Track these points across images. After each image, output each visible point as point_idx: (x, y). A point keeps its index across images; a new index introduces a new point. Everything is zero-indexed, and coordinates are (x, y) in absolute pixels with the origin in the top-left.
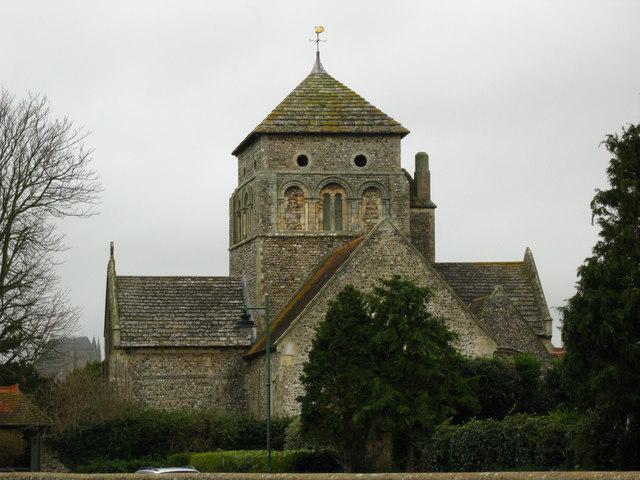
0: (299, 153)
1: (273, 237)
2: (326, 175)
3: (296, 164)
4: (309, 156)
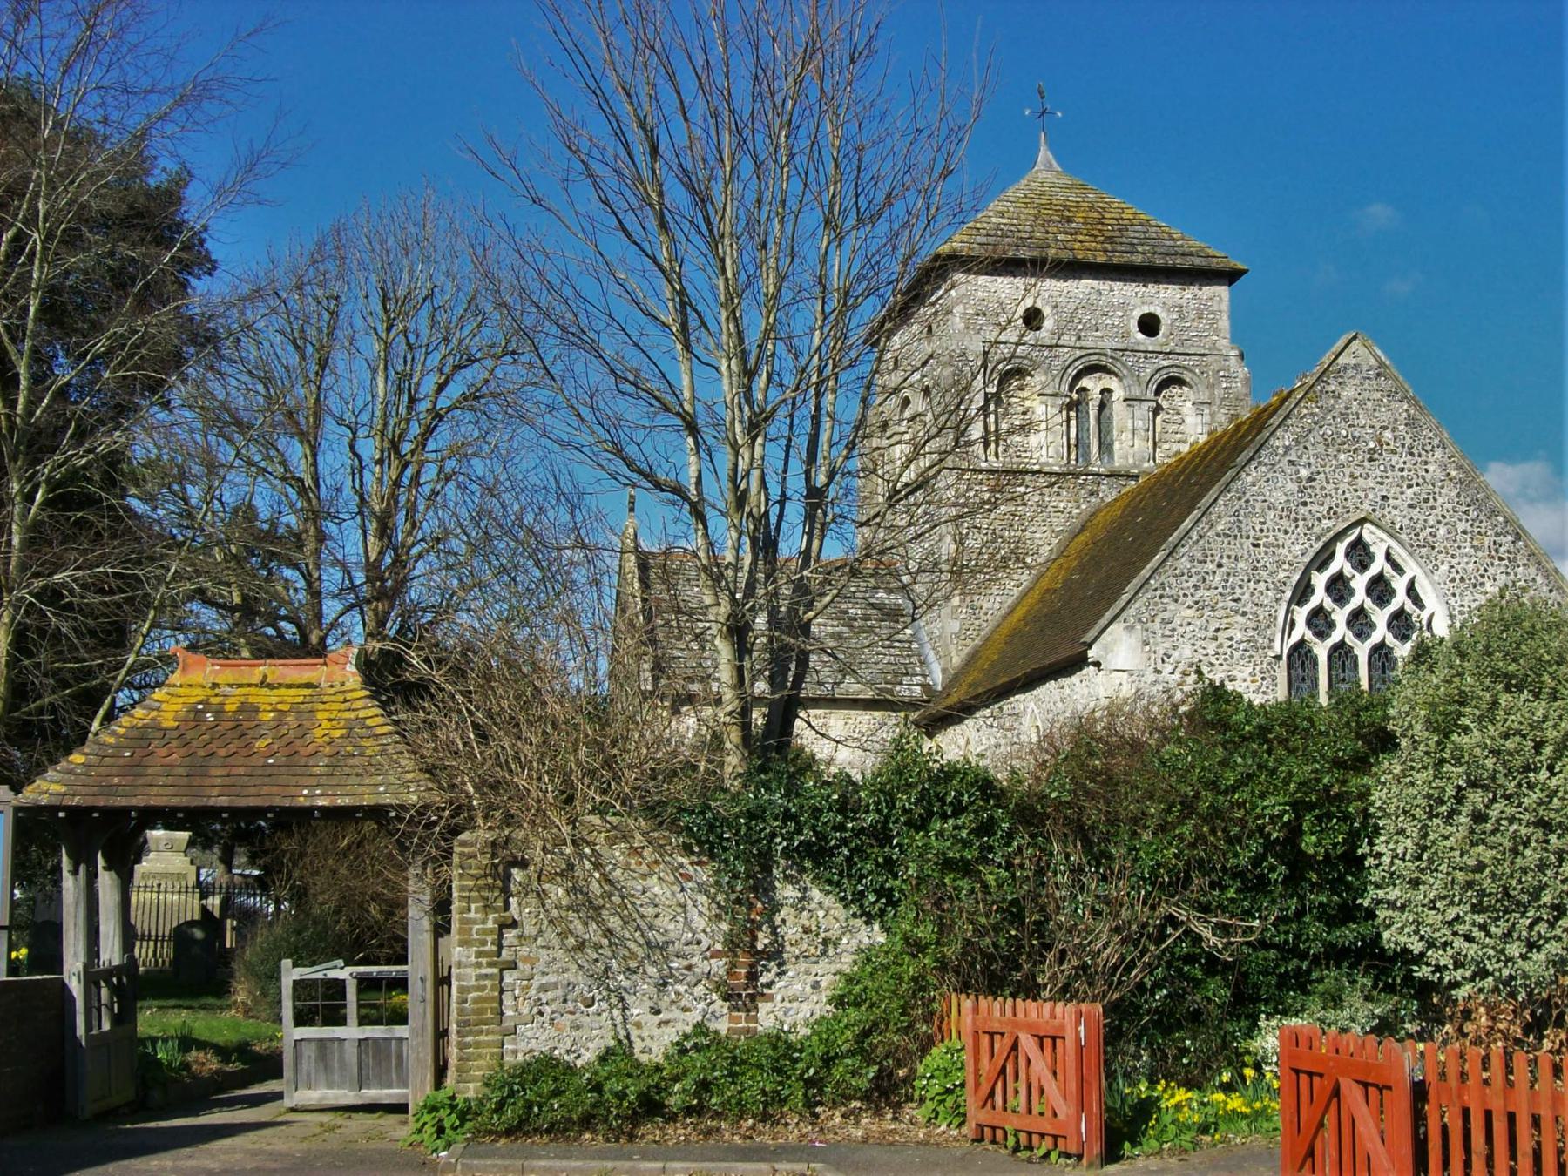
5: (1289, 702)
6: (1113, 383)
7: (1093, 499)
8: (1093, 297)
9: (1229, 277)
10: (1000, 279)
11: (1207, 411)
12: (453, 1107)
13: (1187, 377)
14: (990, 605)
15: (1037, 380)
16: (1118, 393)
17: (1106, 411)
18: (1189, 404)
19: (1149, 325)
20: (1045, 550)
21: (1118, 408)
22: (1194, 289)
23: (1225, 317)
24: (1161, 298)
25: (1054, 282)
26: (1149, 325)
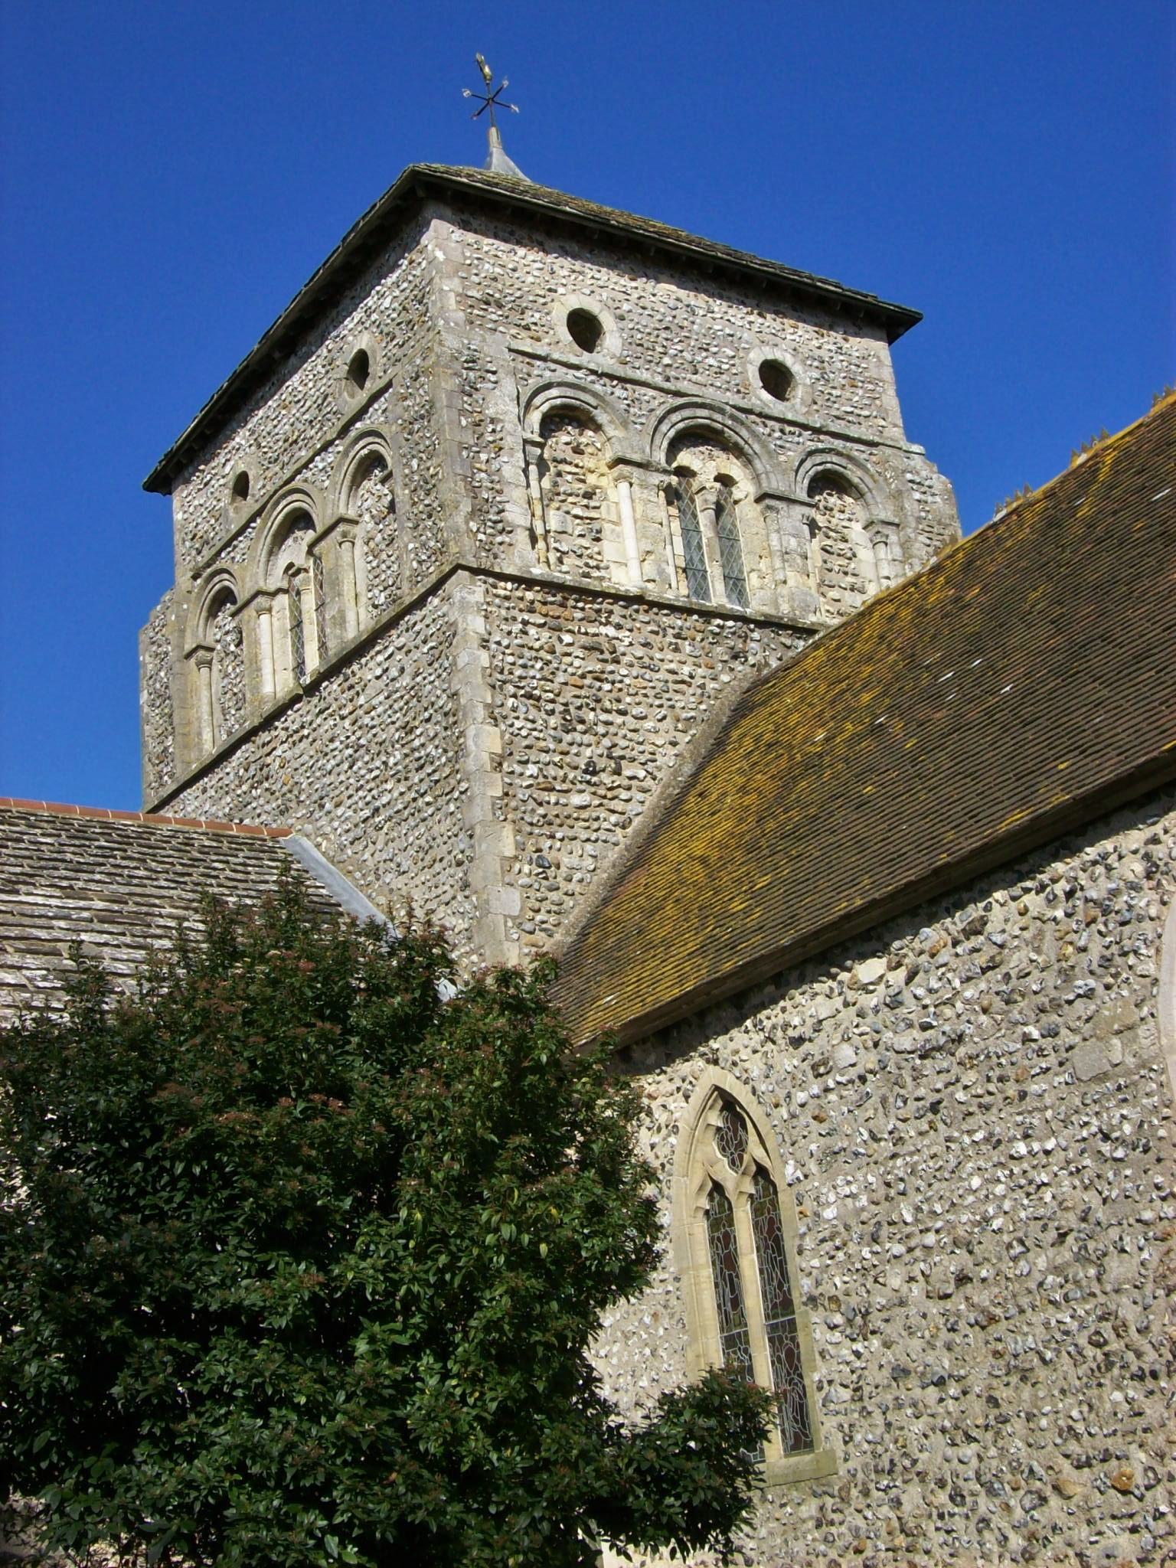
0: (575, 302)
1: (529, 583)
2: (677, 394)
3: (566, 337)
4: (607, 321)
5: (727, 1363)
6: (733, 468)
7: (737, 665)
8: (681, 314)
9: (889, 323)
10: (521, 251)
11: (893, 538)
12: (286, 870)
13: (854, 474)
14: (574, 861)
15: (615, 438)
16: (745, 488)
17: (724, 517)
18: (857, 527)
19: (776, 377)
20: (667, 758)
21: (746, 513)
22: (837, 336)
23: (891, 391)
24: (792, 340)
25: (614, 276)
26: (776, 377)
